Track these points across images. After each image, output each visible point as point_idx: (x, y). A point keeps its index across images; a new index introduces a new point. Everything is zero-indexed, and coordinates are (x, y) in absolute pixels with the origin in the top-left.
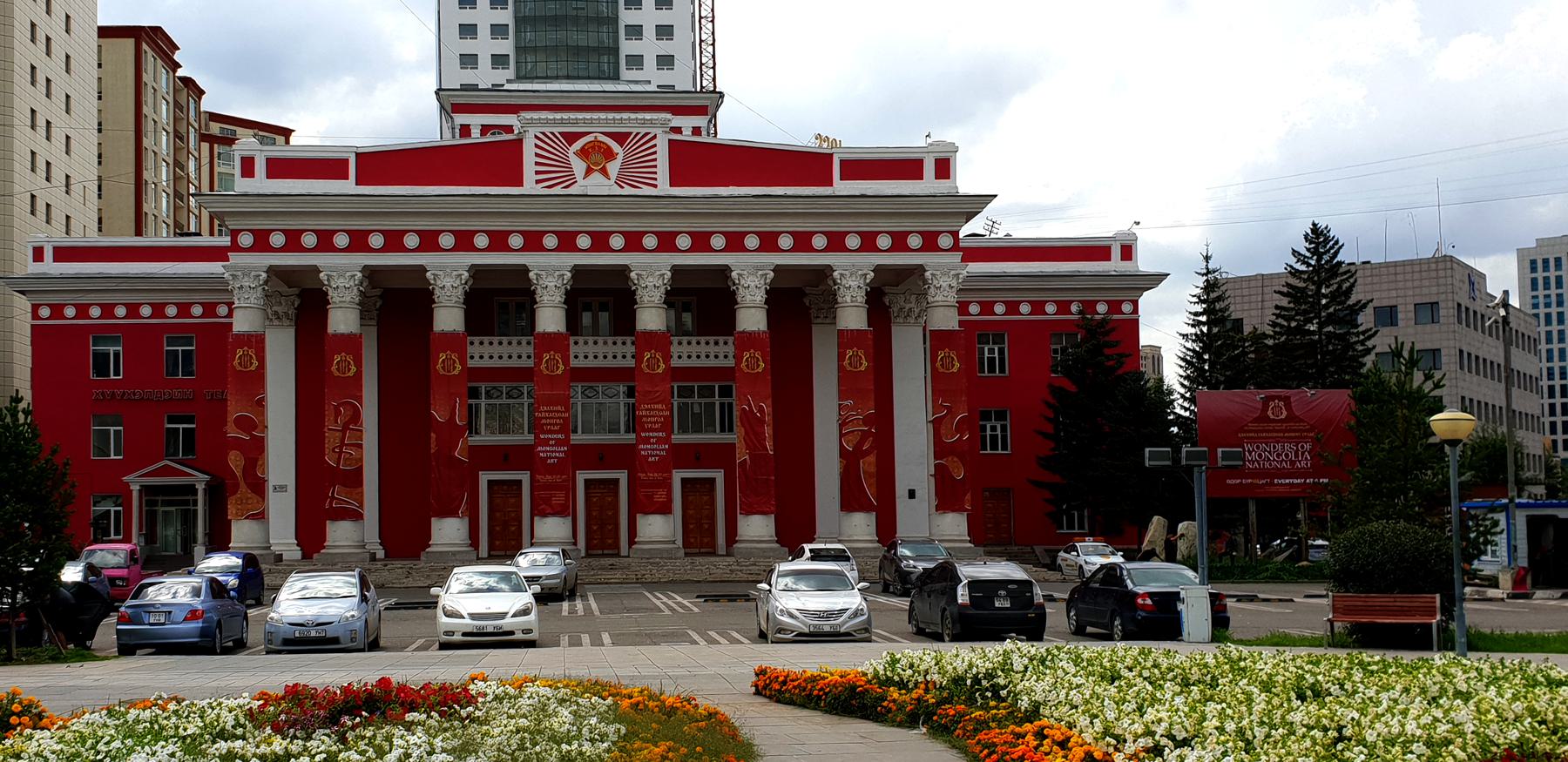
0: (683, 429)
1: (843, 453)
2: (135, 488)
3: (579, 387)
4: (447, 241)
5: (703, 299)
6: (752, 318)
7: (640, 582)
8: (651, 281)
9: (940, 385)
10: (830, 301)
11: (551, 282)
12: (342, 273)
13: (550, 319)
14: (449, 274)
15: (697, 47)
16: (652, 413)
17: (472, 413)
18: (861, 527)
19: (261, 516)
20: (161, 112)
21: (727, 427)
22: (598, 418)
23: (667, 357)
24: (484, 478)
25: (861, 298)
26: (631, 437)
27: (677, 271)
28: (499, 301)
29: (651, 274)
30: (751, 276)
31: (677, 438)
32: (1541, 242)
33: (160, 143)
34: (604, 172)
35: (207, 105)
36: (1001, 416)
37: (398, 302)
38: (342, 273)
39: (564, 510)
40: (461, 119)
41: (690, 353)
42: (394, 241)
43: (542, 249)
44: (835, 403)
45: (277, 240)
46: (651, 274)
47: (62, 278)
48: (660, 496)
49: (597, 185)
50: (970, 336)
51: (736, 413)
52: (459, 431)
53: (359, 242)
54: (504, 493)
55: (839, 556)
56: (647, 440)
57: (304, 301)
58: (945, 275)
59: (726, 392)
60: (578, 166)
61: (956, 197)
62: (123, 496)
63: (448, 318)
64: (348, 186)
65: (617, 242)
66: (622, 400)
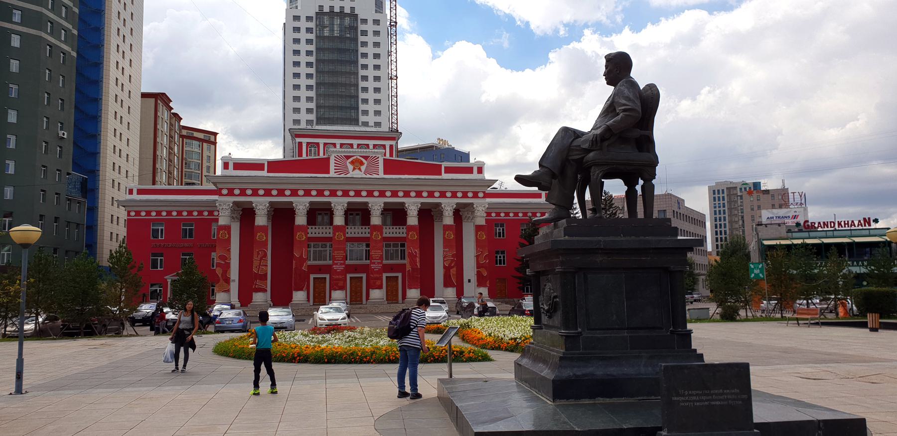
0: (387, 259)
1: (445, 267)
2: (169, 281)
3: (348, 244)
4: (301, 193)
5: (396, 214)
6: (413, 220)
7: (371, 313)
8: (376, 208)
9: (479, 244)
10: (441, 214)
11: (339, 208)
12: (261, 204)
13: (339, 220)
14: (301, 205)
15: (389, 54)
16: (374, 253)
17: (308, 252)
18: (451, 293)
19: (228, 291)
20: (164, 128)
21: (403, 258)
22: (356, 254)
23: (382, 233)
24: (312, 276)
25: (451, 214)
26: (368, 262)
27: (385, 203)
28: (319, 213)
29: (376, 205)
30: (413, 206)
31: (385, 262)
32: (717, 184)
33: (164, 140)
34: (360, 169)
35: (182, 123)
36: (503, 252)
37: (282, 215)
38: (261, 204)
39: (342, 288)
40: (298, 140)
41: (391, 231)
42: (281, 193)
43: (330, 190)
44: (442, 250)
45: (237, 192)
46: (376, 205)
47: (140, 201)
48: (378, 283)
49: (357, 174)
50: (491, 224)
51: (406, 254)
52: (305, 260)
53: (268, 193)
54: (320, 282)
55: (442, 302)
56: (374, 263)
57: (246, 214)
58: (481, 206)
59: (403, 245)
60: (350, 167)
61: (484, 180)
62: (164, 284)
63: (301, 220)
64: (264, 173)
65: (364, 194)
66: (364, 248)
